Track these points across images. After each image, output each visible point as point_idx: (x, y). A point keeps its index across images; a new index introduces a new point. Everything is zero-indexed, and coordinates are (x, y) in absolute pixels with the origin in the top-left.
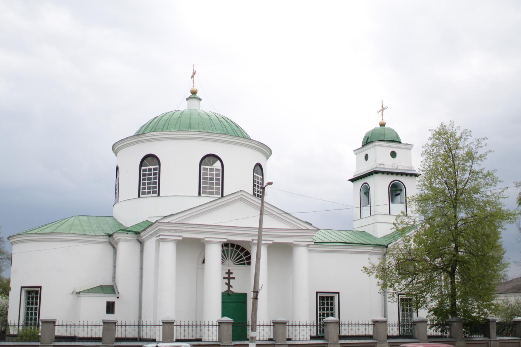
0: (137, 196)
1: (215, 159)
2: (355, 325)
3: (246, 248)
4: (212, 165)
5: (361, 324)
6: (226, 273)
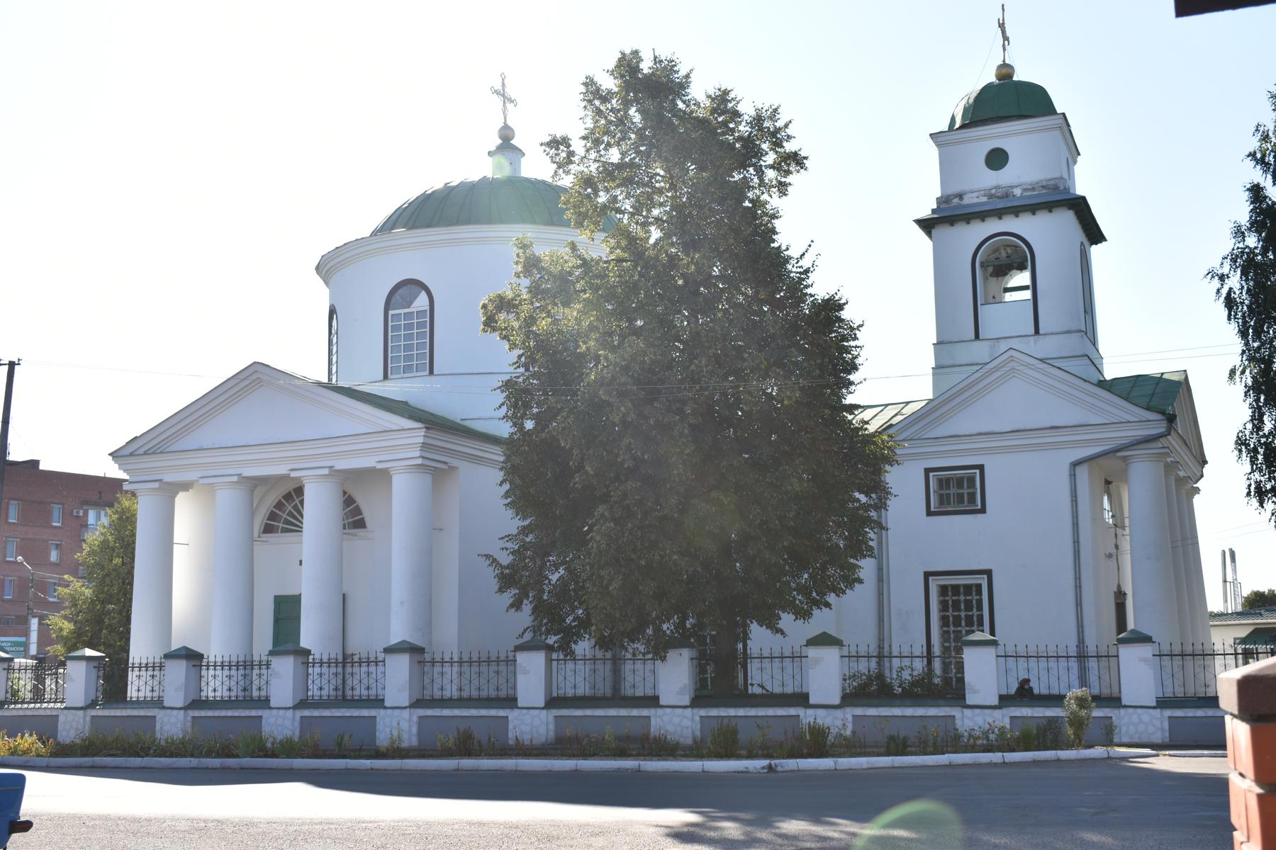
0: (381, 376)
1: (414, 288)
2: (489, 661)
3: (288, 491)
4: (410, 305)
5: (897, 654)
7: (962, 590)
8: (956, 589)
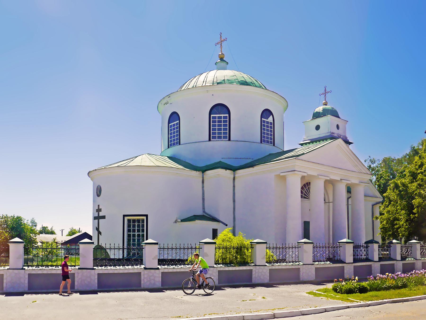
7: (129, 233)
8: (134, 221)
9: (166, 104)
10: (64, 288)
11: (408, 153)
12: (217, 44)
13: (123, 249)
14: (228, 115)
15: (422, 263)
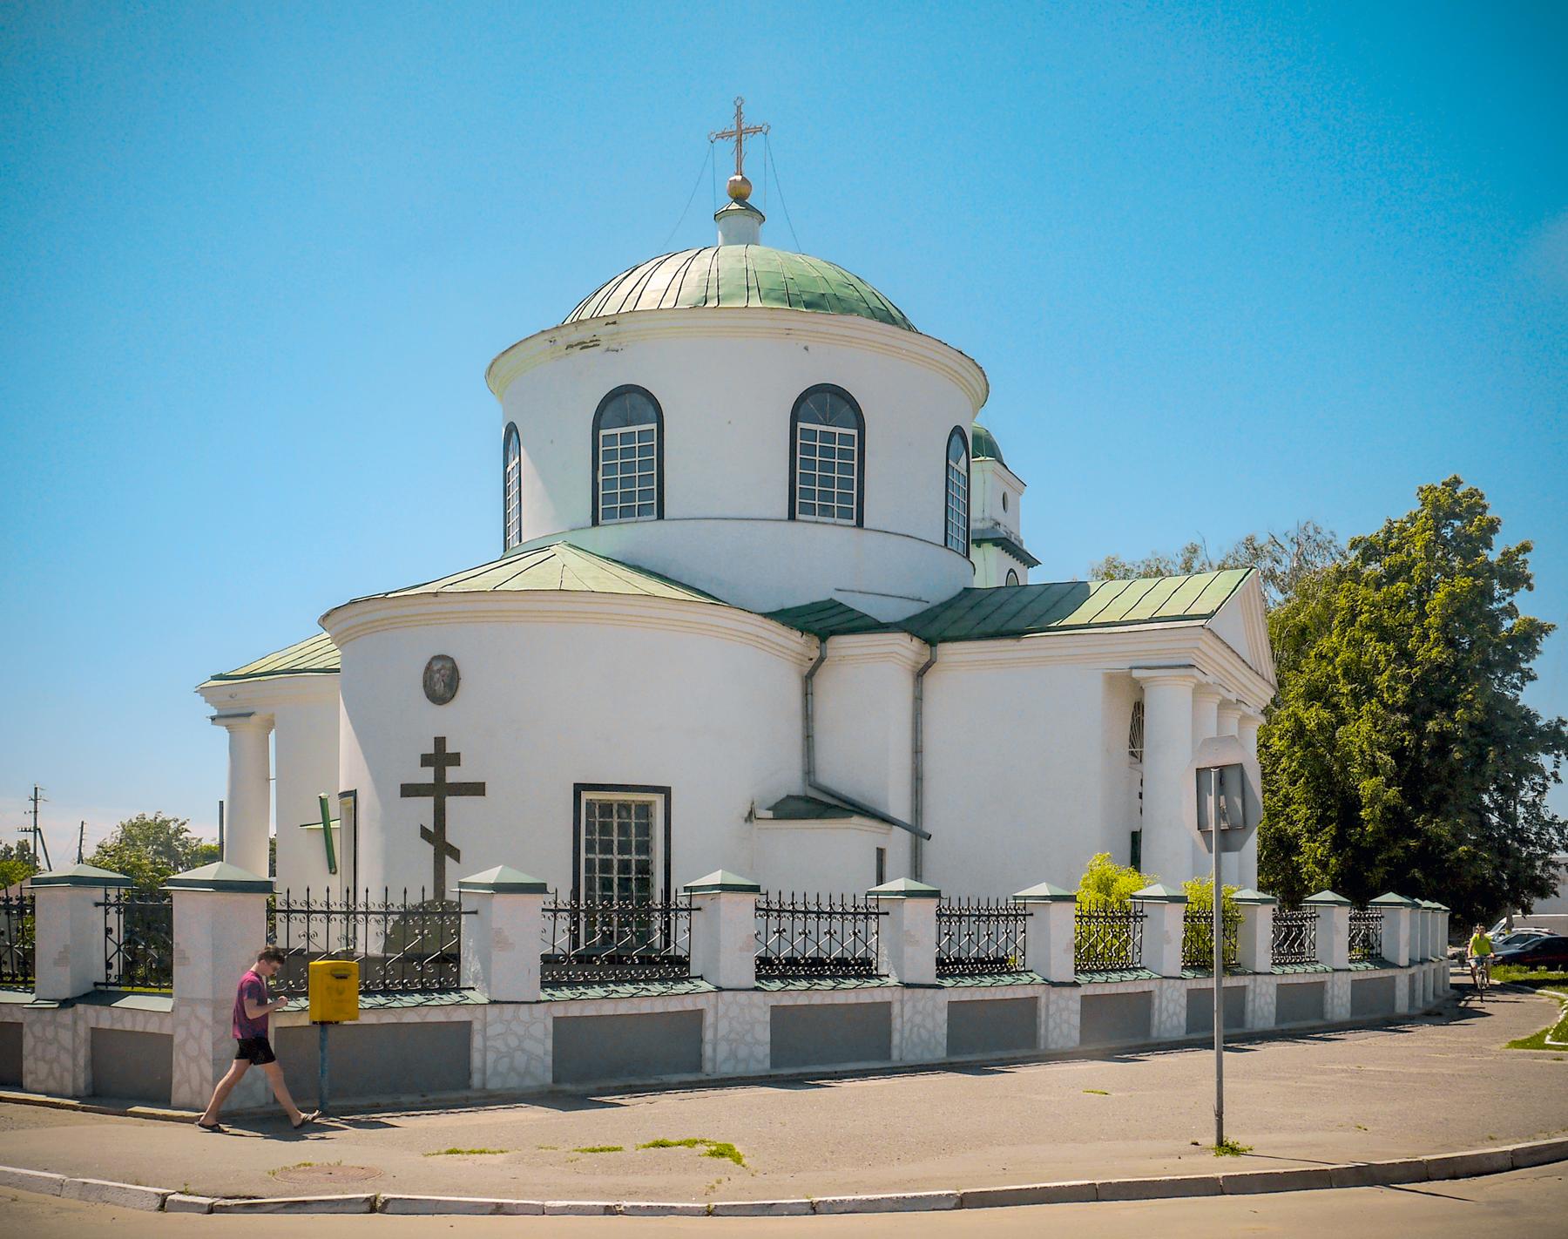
6: (426, 760)
7: (644, 857)
9: (580, 347)
10: (1227, 1024)
11: (1545, 638)
12: (722, 136)
13: (574, 913)
14: (856, 431)
15: (1190, 991)
